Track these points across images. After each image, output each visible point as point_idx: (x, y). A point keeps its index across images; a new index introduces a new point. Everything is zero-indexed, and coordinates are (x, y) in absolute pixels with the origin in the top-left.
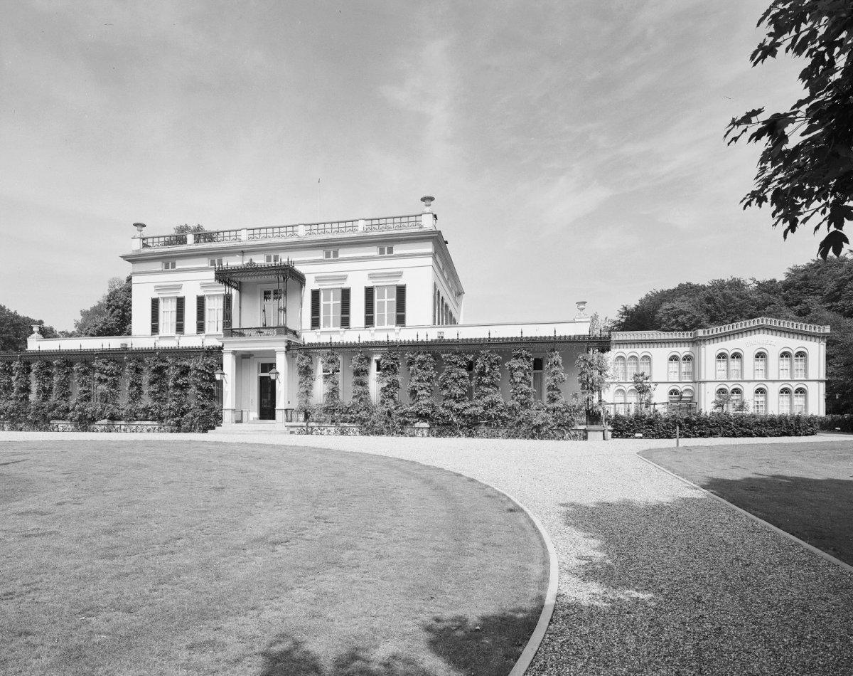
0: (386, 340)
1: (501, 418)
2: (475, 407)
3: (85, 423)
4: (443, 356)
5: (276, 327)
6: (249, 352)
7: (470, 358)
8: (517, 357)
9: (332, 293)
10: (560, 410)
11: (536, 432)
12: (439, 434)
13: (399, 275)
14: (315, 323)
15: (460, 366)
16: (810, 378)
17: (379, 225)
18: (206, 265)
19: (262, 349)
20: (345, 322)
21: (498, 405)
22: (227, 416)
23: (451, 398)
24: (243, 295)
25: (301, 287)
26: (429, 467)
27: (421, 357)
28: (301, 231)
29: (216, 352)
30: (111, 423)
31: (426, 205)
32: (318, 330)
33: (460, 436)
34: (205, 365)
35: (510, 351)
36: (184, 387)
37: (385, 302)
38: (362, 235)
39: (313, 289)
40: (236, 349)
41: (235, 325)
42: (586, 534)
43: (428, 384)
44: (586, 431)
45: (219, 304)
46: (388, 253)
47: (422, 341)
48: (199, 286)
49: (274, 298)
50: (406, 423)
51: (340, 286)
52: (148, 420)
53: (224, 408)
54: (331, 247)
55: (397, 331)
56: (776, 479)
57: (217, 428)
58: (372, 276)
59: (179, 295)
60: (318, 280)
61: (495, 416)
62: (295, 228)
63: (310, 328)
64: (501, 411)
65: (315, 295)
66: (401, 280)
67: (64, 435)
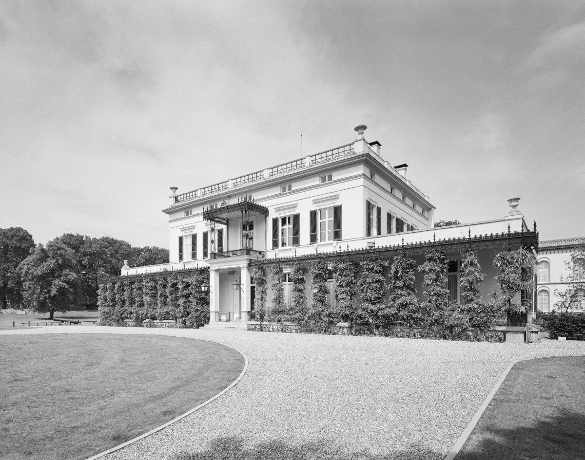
0: (506, 232)
1: (413, 318)
2: (387, 309)
3: (139, 322)
4: (361, 263)
5: (240, 250)
6: (233, 269)
7: (386, 264)
8: (430, 260)
9: (327, 212)
10: (474, 311)
11: (449, 332)
12: (359, 333)
13: (336, 197)
14: (275, 244)
15: (376, 271)
17: (344, 151)
18: (279, 192)
19: (232, 266)
20: (296, 241)
21: (411, 307)
22: (212, 316)
23: (367, 300)
24: (230, 229)
25: (266, 218)
27: (341, 266)
28: (266, 175)
29: (205, 272)
30: (151, 321)
31: (359, 134)
32: (277, 249)
33: (375, 335)
34: (197, 281)
35: (423, 256)
36: (187, 296)
37: (326, 221)
38: (201, 198)
39: (274, 217)
40: (216, 268)
41: (225, 250)
43: (349, 289)
44: (505, 333)
45: (215, 236)
47: (516, 233)
48: (180, 230)
50: (331, 323)
51: (332, 205)
52: (502, 331)
53: (211, 311)
54: (285, 183)
55: (335, 245)
56: (166, 343)
57: (205, 325)
58: (315, 202)
59: (336, 205)
60: (277, 210)
61: (407, 316)
62: (352, 146)
63: (309, 244)
64: (414, 312)
65: (275, 221)
66: (296, 210)
67: (130, 330)
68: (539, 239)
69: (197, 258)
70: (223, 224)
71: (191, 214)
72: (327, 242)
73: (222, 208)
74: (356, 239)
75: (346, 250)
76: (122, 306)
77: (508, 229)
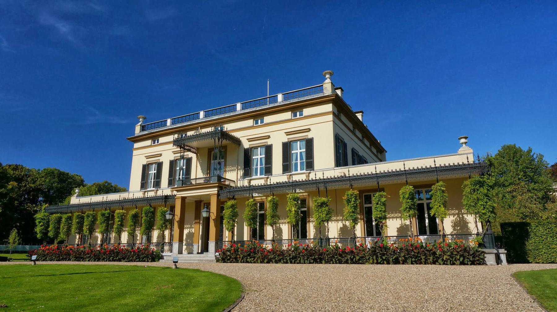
37: (298, 150)
45: (182, 163)
68: (169, 195)
69: (315, 168)
70: (193, 152)
71: (158, 142)
72: (259, 176)
73: (194, 135)
74: (328, 170)
75: (322, 178)
76: (546, 299)
77: (348, 172)
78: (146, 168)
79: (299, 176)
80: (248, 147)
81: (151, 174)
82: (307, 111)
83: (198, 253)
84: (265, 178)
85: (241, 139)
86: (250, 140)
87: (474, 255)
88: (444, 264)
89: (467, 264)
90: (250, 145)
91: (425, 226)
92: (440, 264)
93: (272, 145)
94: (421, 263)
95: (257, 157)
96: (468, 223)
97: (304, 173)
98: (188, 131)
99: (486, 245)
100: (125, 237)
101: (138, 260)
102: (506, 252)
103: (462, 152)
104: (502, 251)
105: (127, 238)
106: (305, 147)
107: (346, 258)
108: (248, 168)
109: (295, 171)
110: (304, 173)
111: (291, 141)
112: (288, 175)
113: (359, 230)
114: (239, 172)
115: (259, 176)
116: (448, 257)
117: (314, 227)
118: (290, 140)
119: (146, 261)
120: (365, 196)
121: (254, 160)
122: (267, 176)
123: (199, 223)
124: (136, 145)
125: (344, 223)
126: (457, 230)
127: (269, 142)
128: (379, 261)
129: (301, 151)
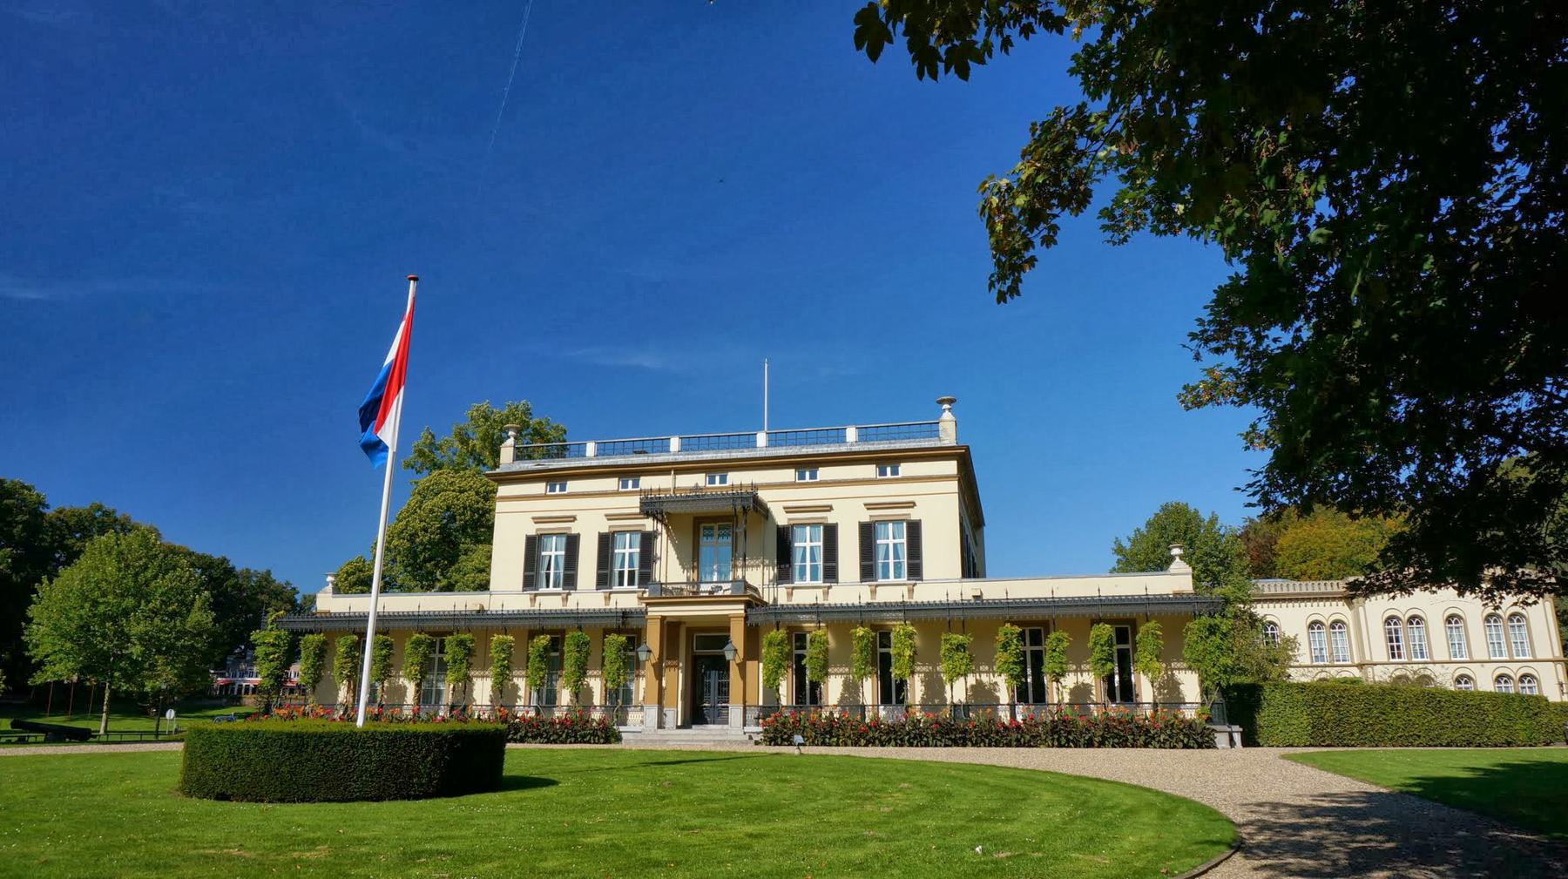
16: (1476, 658)
20: (831, 574)
26: (1079, 778)
42: (1257, 863)
46: (892, 475)
49: (719, 535)
63: (521, 589)
69: (840, 580)
78: (533, 545)
79: (891, 592)
80: (786, 524)
81: (620, 556)
82: (906, 469)
83: (678, 727)
84: (825, 587)
85: (769, 505)
86: (788, 510)
87: (1202, 734)
88: (1160, 747)
89: (1193, 748)
90: (789, 519)
91: (1114, 687)
92: (1155, 747)
93: (579, 535)
94: (1126, 746)
95: (802, 544)
96: (1180, 684)
97: (559, 594)
98: (730, 471)
99: (1215, 720)
100: (483, 691)
101: (573, 739)
102: (1241, 730)
103: (1175, 571)
104: (1236, 728)
105: (491, 693)
106: (564, 547)
107: (1009, 738)
108: (788, 566)
109: (883, 578)
110: (559, 594)
111: (541, 535)
112: (606, 592)
113: (869, 690)
114: (766, 572)
115: (551, 589)
116: (1167, 737)
117: (922, 682)
118: (792, 522)
119: (592, 741)
120: (1040, 631)
121: (798, 549)
122: (829, 584)
123: (677, 666)
124: (503, 490)
125: (978, 677)
126: (1164, 694)
127: (575, 528)
128: (1063, 743)
129: (632, 550)
